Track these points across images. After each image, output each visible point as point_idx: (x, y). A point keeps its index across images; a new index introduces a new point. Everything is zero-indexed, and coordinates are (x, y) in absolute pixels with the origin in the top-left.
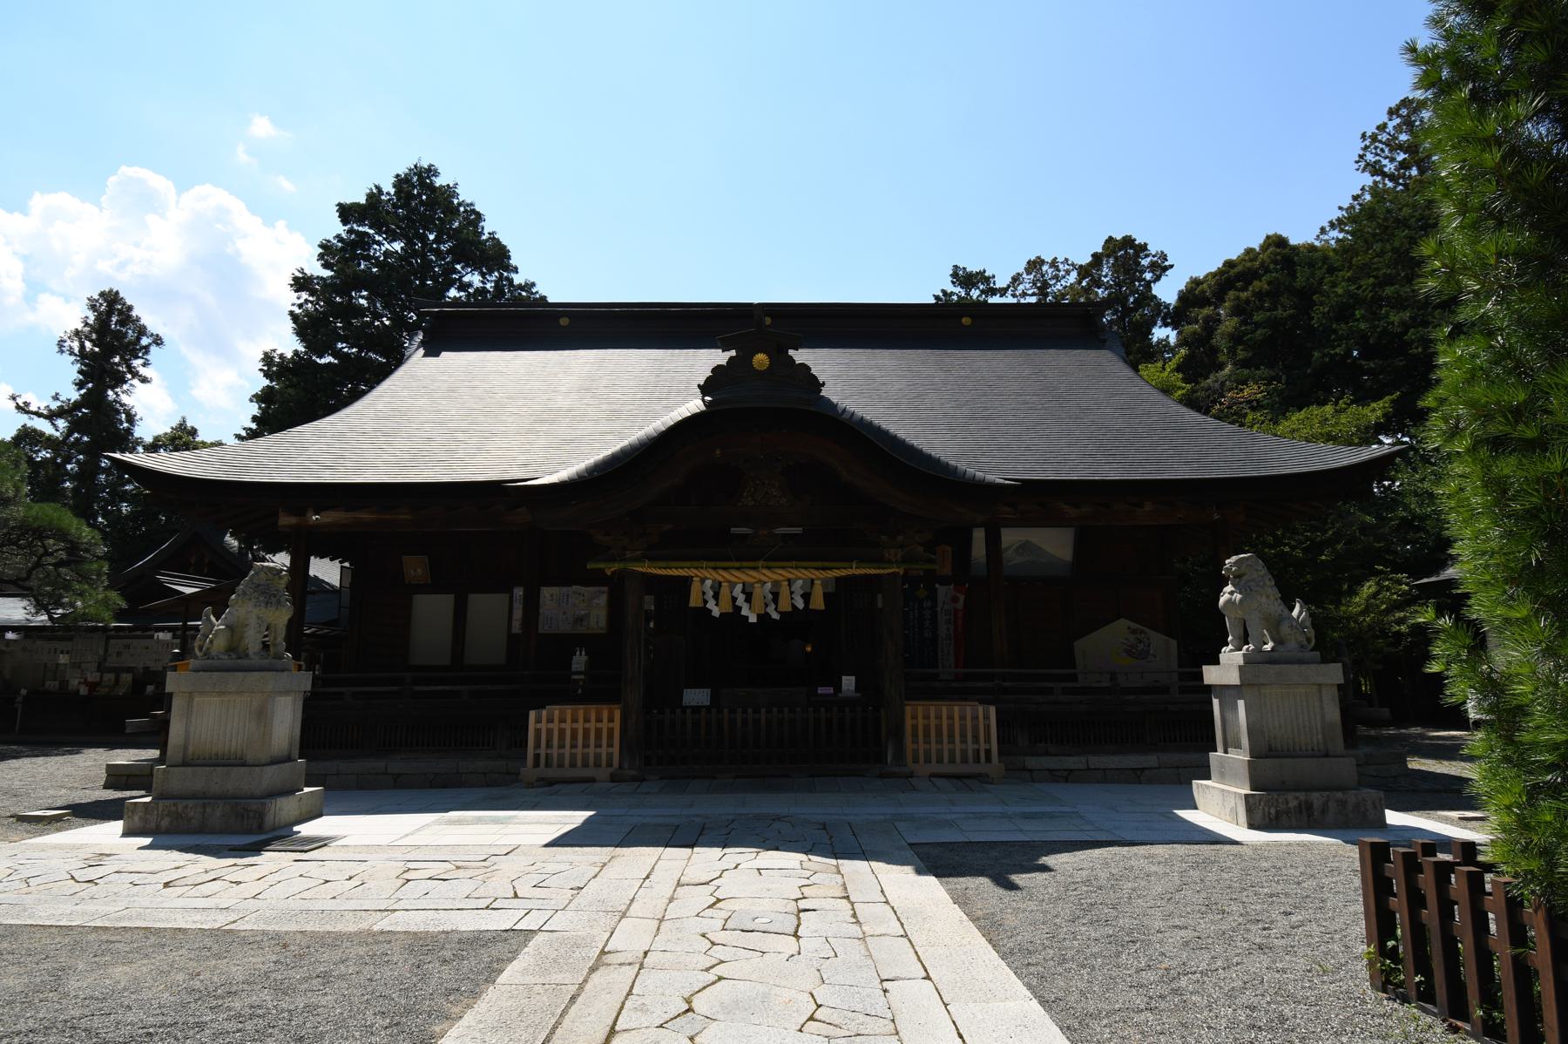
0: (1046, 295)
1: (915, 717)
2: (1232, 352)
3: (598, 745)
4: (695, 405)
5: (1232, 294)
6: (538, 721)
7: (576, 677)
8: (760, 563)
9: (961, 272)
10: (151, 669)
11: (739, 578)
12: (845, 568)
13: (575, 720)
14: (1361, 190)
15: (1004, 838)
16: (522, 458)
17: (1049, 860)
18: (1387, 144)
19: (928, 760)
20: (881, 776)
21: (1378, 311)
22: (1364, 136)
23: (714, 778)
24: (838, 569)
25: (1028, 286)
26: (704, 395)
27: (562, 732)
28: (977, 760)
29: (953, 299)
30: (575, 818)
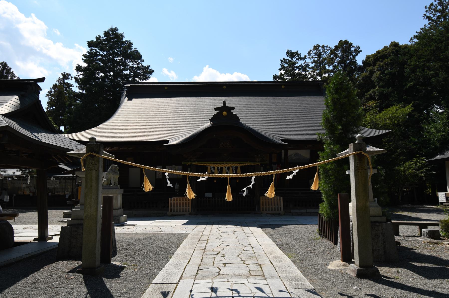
0: (320, 58)
1: (263, 200)
2: (379, 82)
3: (186, 207)
4: (208, 124)
5: (378, 63)
6: (171, 201)
7: (176, 190)
8: (225, 162)
9: (290, 52)
10: (49, 188)
11: (219, 166)
12: (246, 163)
13: (180, 201)
14: (424, 26)
15: (279, 224)
16: (162, 134)
17: (284, 226)
18: (434, 9)
19: (266, 210)
22: (426, 7)
24: (244, 163)
25: (314, 55)
26: (211, 122)
27: (177, 203)
28: (278, 210)
29: (287, 61)
30: (186, 221)
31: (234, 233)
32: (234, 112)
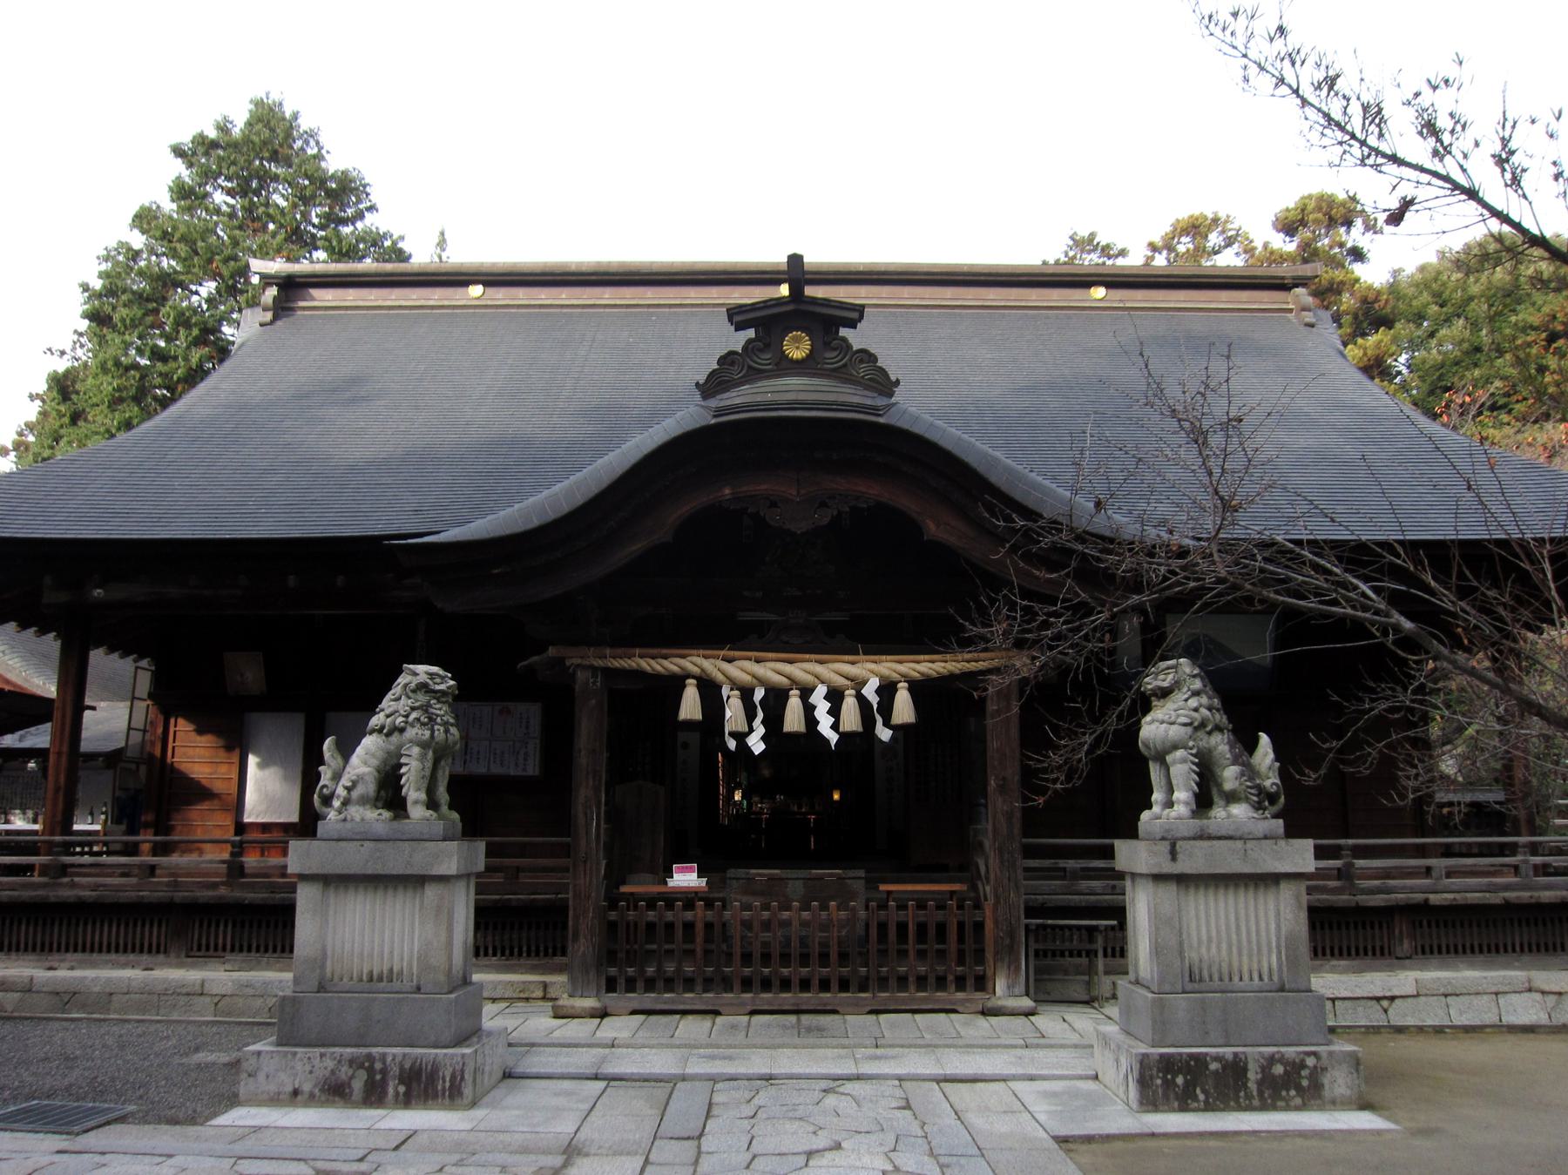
20: (985, 1013)
21: (238, 189)
23: (717, 1013)
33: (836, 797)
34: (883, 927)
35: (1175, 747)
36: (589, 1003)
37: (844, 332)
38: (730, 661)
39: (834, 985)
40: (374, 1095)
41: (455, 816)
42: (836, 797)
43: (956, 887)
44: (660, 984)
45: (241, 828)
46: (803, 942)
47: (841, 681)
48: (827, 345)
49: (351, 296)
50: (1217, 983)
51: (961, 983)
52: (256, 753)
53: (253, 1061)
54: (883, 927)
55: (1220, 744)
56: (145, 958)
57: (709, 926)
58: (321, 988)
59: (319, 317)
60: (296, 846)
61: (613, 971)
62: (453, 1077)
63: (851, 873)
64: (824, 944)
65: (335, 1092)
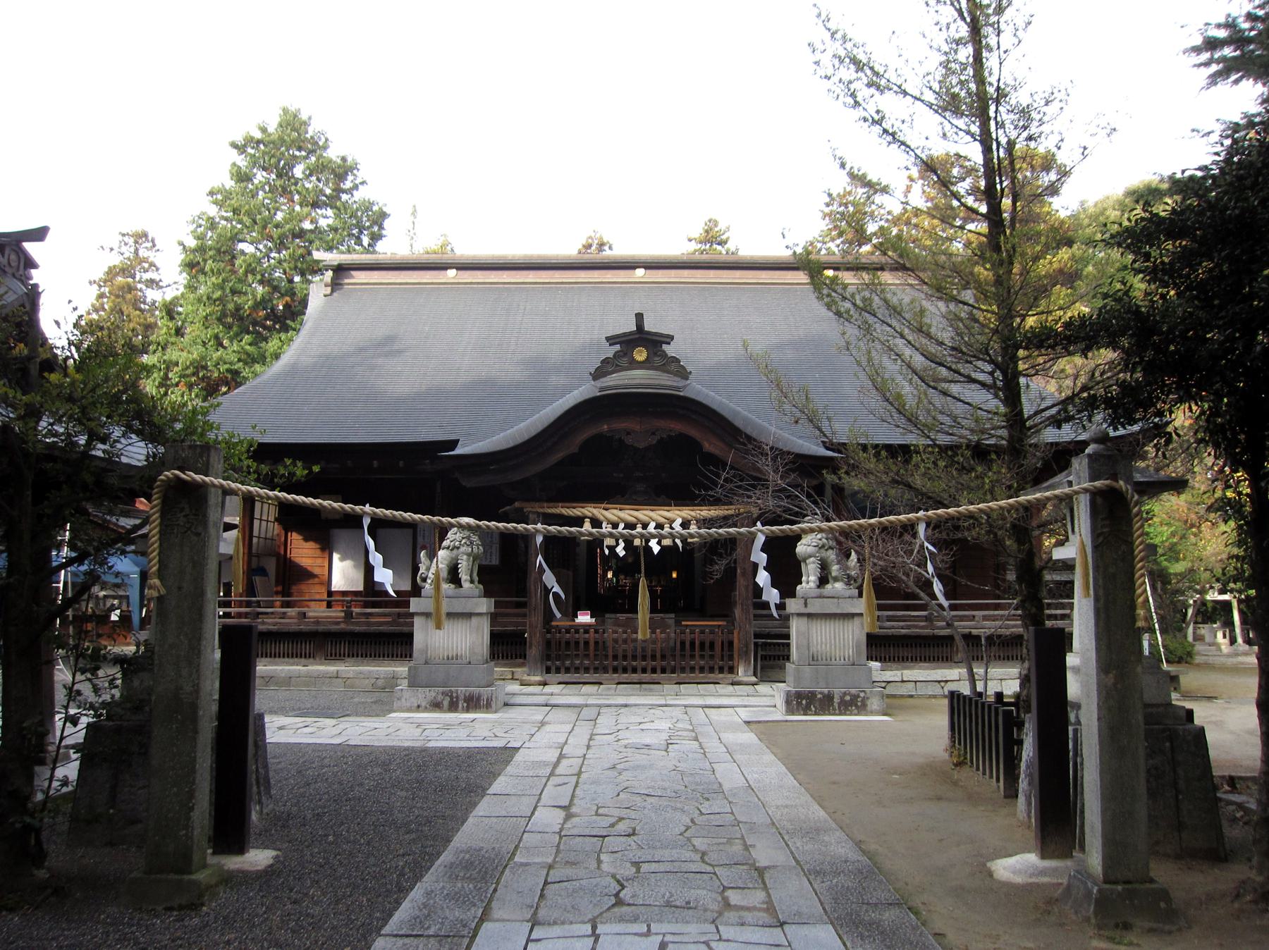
31: (666, 751)
32: (670, 350)
33: (674, 575)
34: (683, 643)
35: (810, 557)
36: (538, 678)
37: (665, 347)
38: (607, 509)
39: (659, 670)
40: (453, 707)
41: (481, 587)
42: (674, 575)
43: (720, 623)
44: (573, 670)
45: (330, 593)
46: (644, 649)
47: (663, 520)
48: (655, 354)
49: (375, 277)
50: (824, 662)
51: (721, 670)
52: (338, 552)
53: (399, 693)
54: (683, 643)
55: (832, 555)
56: (303, 660)
57: (596, 643)
58: (426, 663)
59: (360, 290)
60: (413, 601)
61: (549, 663)
62: (487, 700)
63: (668, 616)
64: (654, 651)
65: (436, 706)
